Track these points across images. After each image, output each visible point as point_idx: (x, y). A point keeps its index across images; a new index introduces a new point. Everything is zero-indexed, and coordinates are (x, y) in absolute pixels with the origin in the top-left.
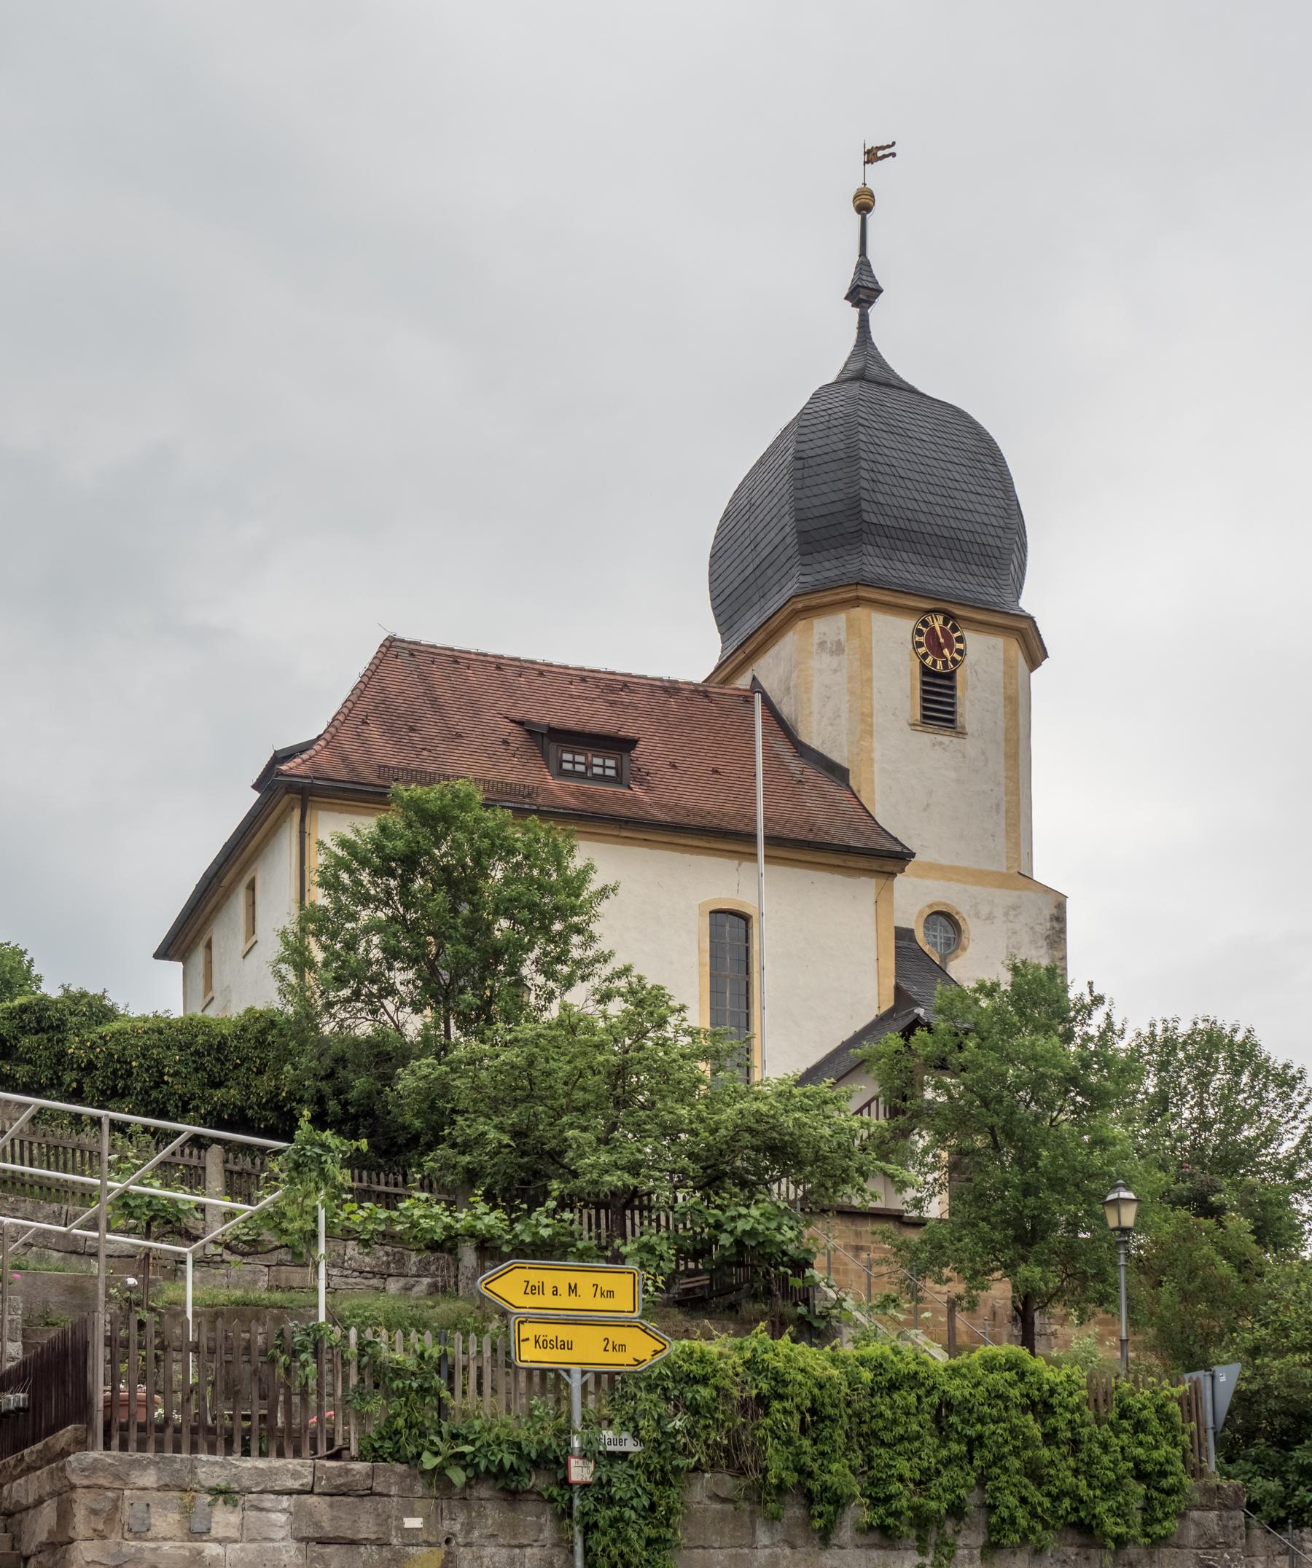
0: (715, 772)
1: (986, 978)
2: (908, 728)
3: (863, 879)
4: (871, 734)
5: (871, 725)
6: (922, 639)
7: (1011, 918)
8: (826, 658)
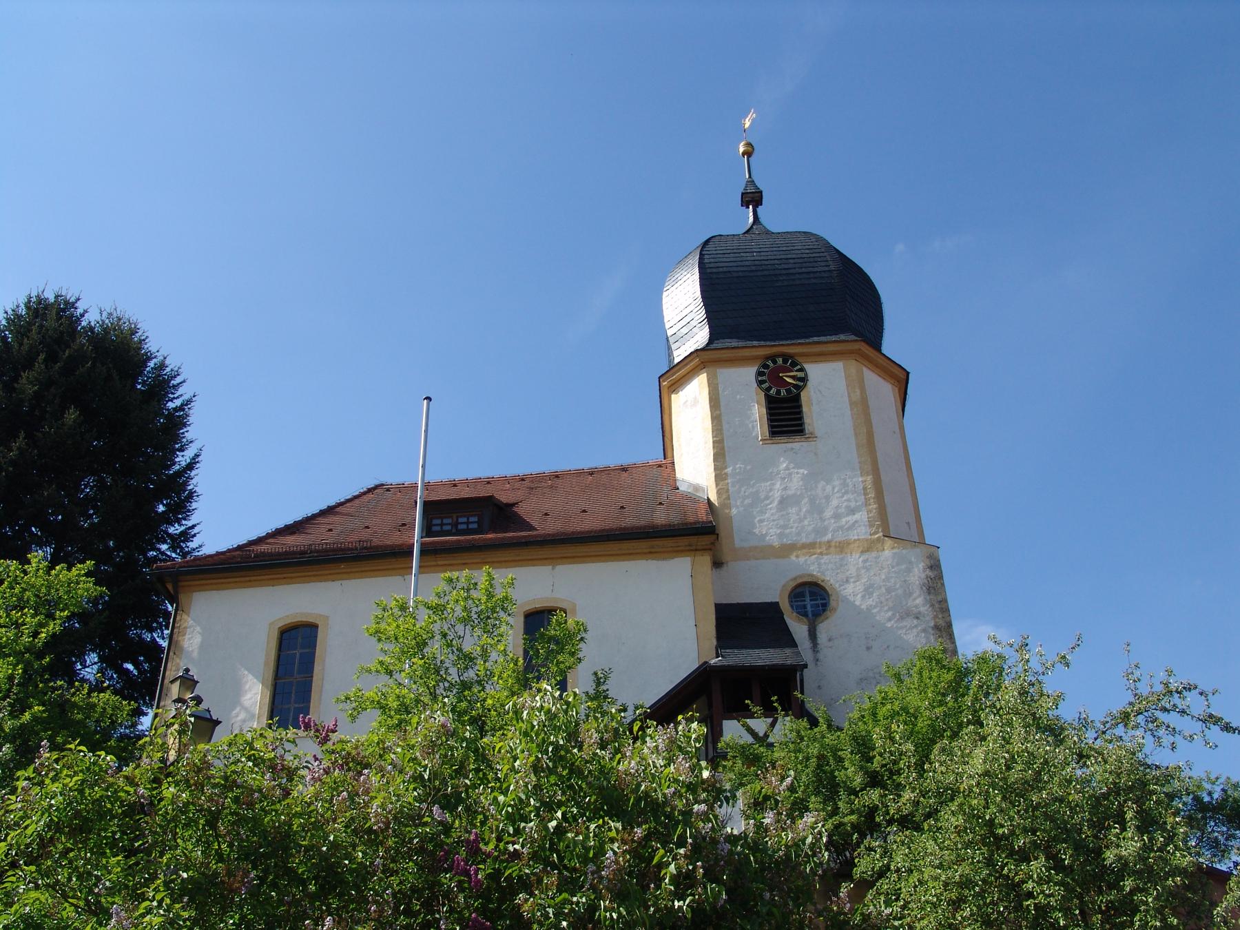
1: (185, 392)
3: (676, 560)
6: (764, 378)
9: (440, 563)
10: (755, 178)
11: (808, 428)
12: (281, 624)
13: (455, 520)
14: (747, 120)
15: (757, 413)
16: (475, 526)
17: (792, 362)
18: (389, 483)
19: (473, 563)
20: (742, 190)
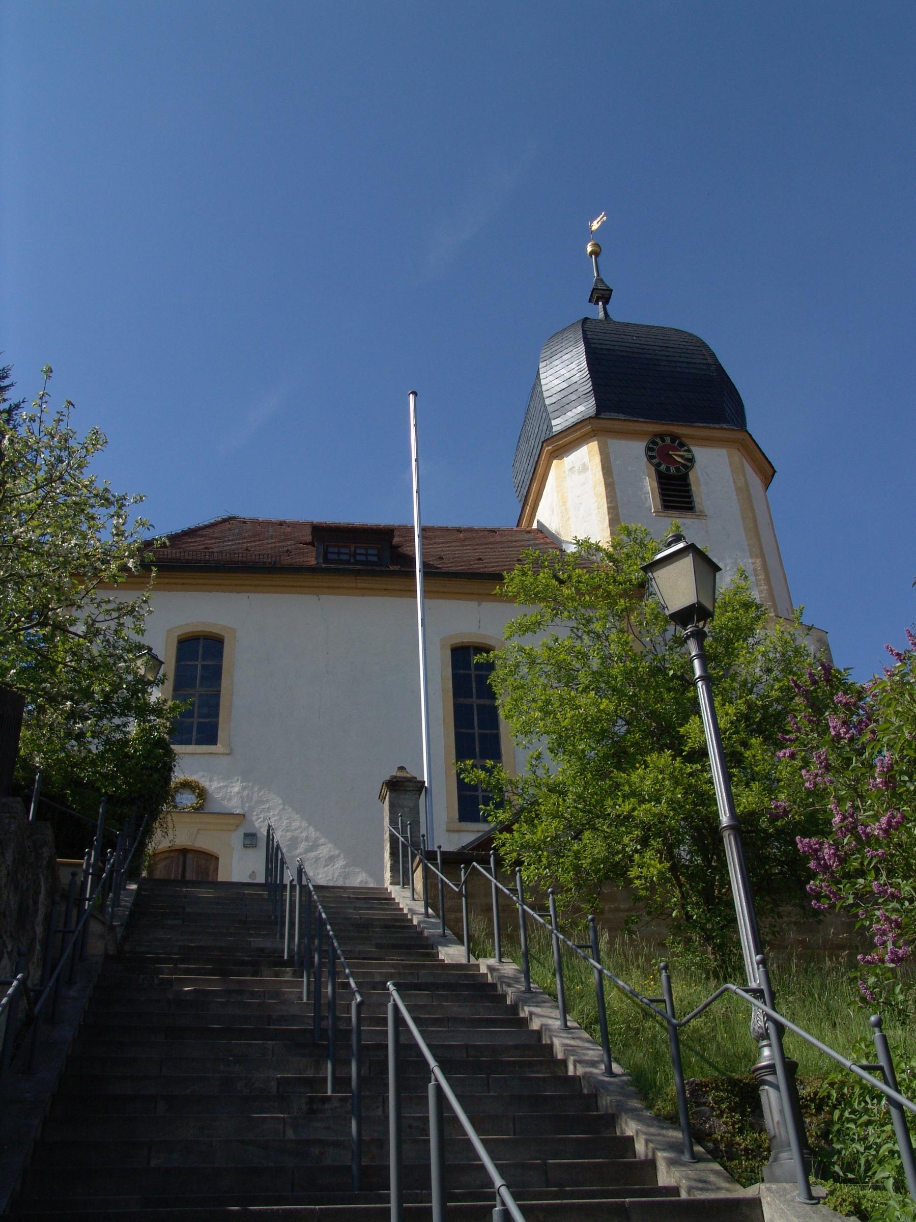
0: (480, 559)
6: (653, 453)
9: (360, 585)
10: (602, 276)
11: (697, 506)
12: (179, 632)
13: (353, 549)
14: (595, 222)
15: (649, 486)
16: (375, 559)
17: (679, 443)
18: (240, 516)
19: (395, 590)
20: (593, 286)
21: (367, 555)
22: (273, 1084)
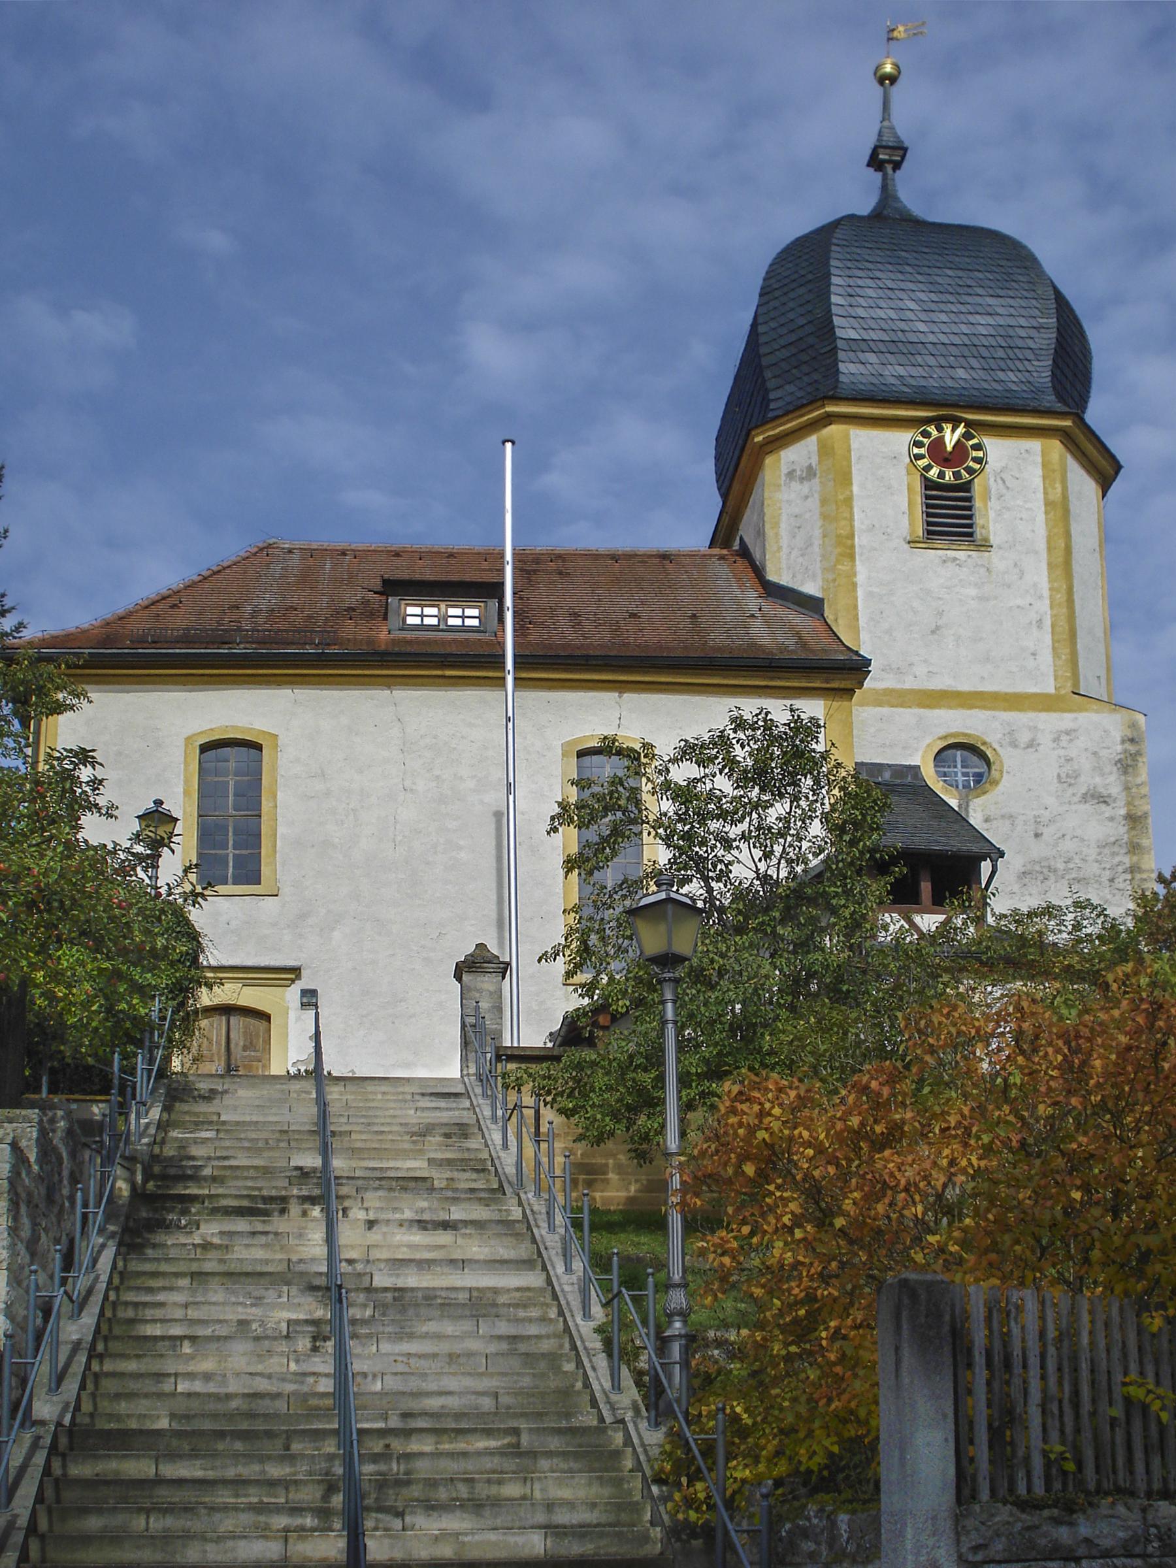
0: (633, 615)
2: (907, 546)
4: (852, 557)
5: (853, 547)
7: (1064, 744)
8: (796, 485)
11: (979, 533)
21: (463, 617)
22: (284, 1326)
